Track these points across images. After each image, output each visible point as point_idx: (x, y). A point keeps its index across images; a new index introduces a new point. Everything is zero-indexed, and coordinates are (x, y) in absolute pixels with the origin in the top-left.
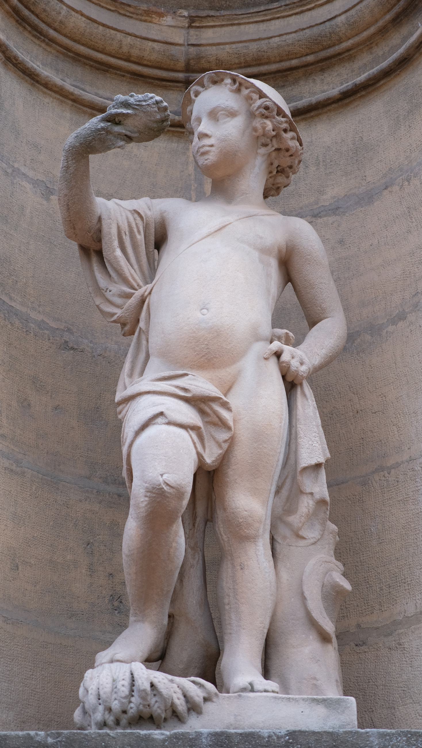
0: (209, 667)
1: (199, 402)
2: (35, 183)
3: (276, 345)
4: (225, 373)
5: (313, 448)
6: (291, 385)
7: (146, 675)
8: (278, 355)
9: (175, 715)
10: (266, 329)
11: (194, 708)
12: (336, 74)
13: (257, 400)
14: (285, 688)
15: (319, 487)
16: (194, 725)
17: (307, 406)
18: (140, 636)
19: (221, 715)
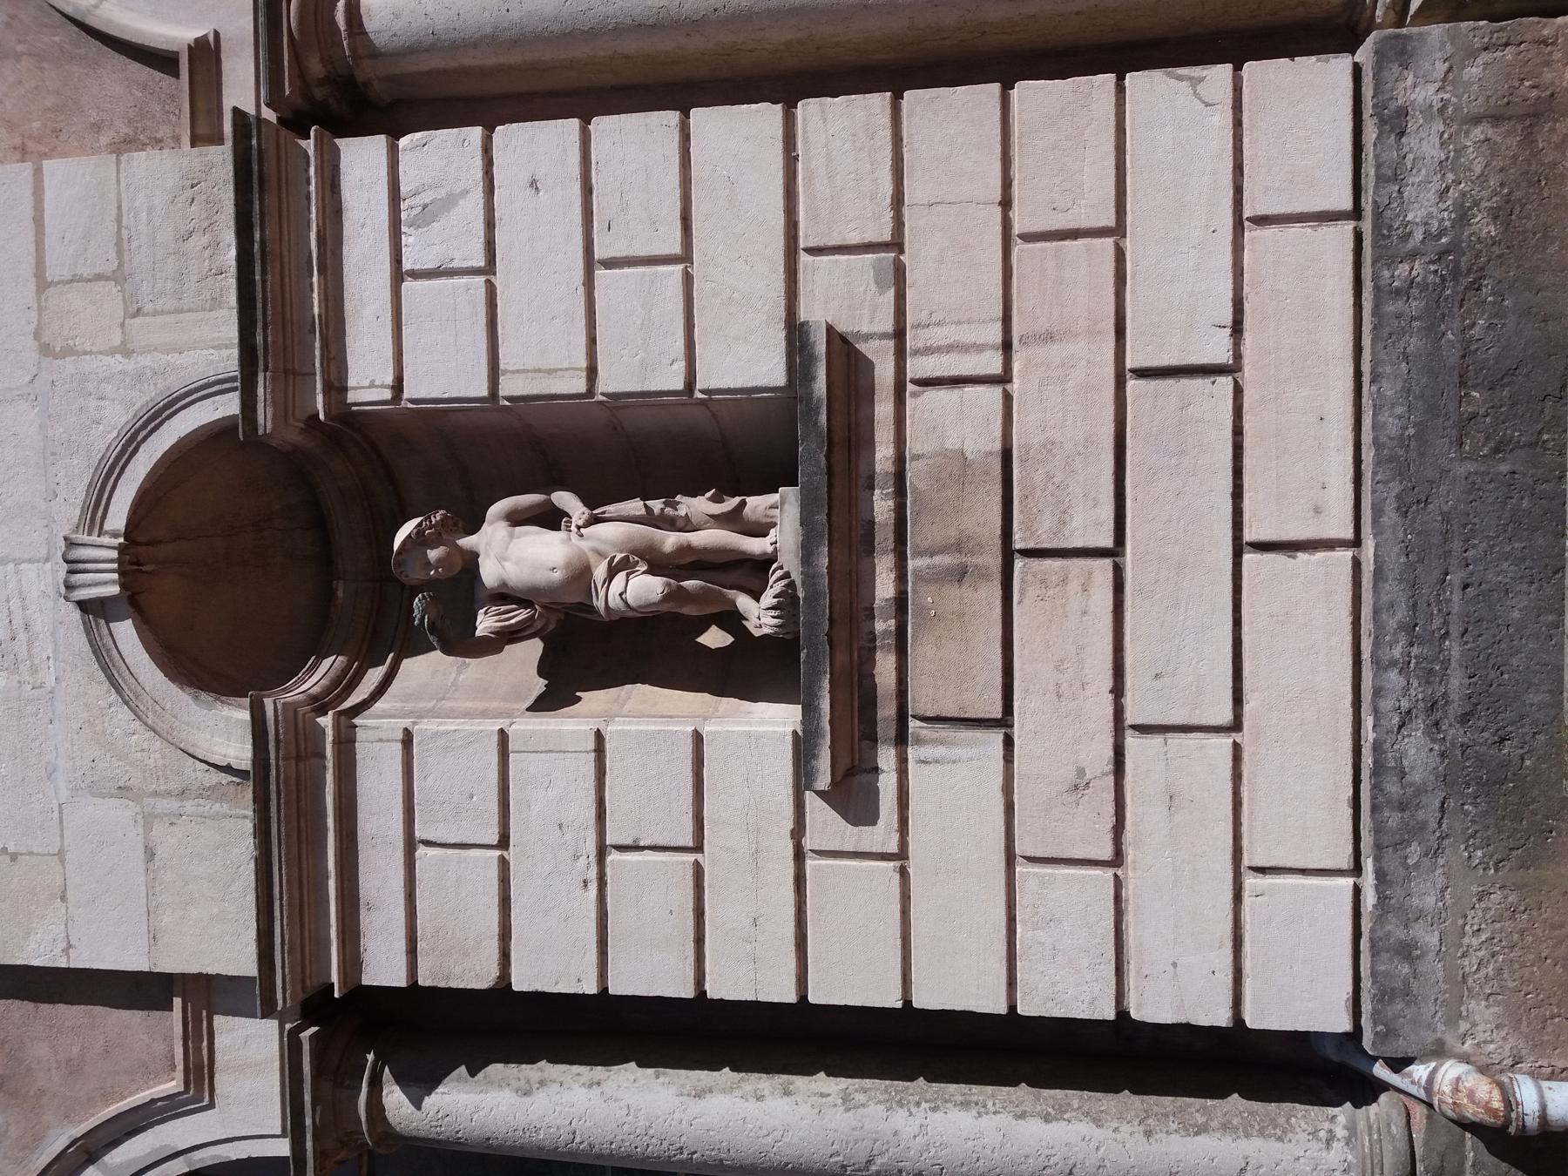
0: (763, 565)
1: (612, 573)
2: (459, 673)
3: (573, 528)
4: (593, 558)
5: (635, 506)
6: (595, 520)
7: (768, 599)
8: (579, 528)
9: (792, 585)
10: (561, 535)
11: (787, 575)
12: (948, 1151)
13: (611, 535)
14: (774, 525)
15: (657, 505)
16: (796, 577)
17: (612, 509)
18: (743, 602)
19: (790, 561)
